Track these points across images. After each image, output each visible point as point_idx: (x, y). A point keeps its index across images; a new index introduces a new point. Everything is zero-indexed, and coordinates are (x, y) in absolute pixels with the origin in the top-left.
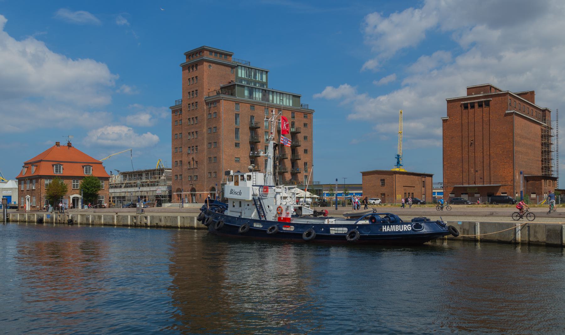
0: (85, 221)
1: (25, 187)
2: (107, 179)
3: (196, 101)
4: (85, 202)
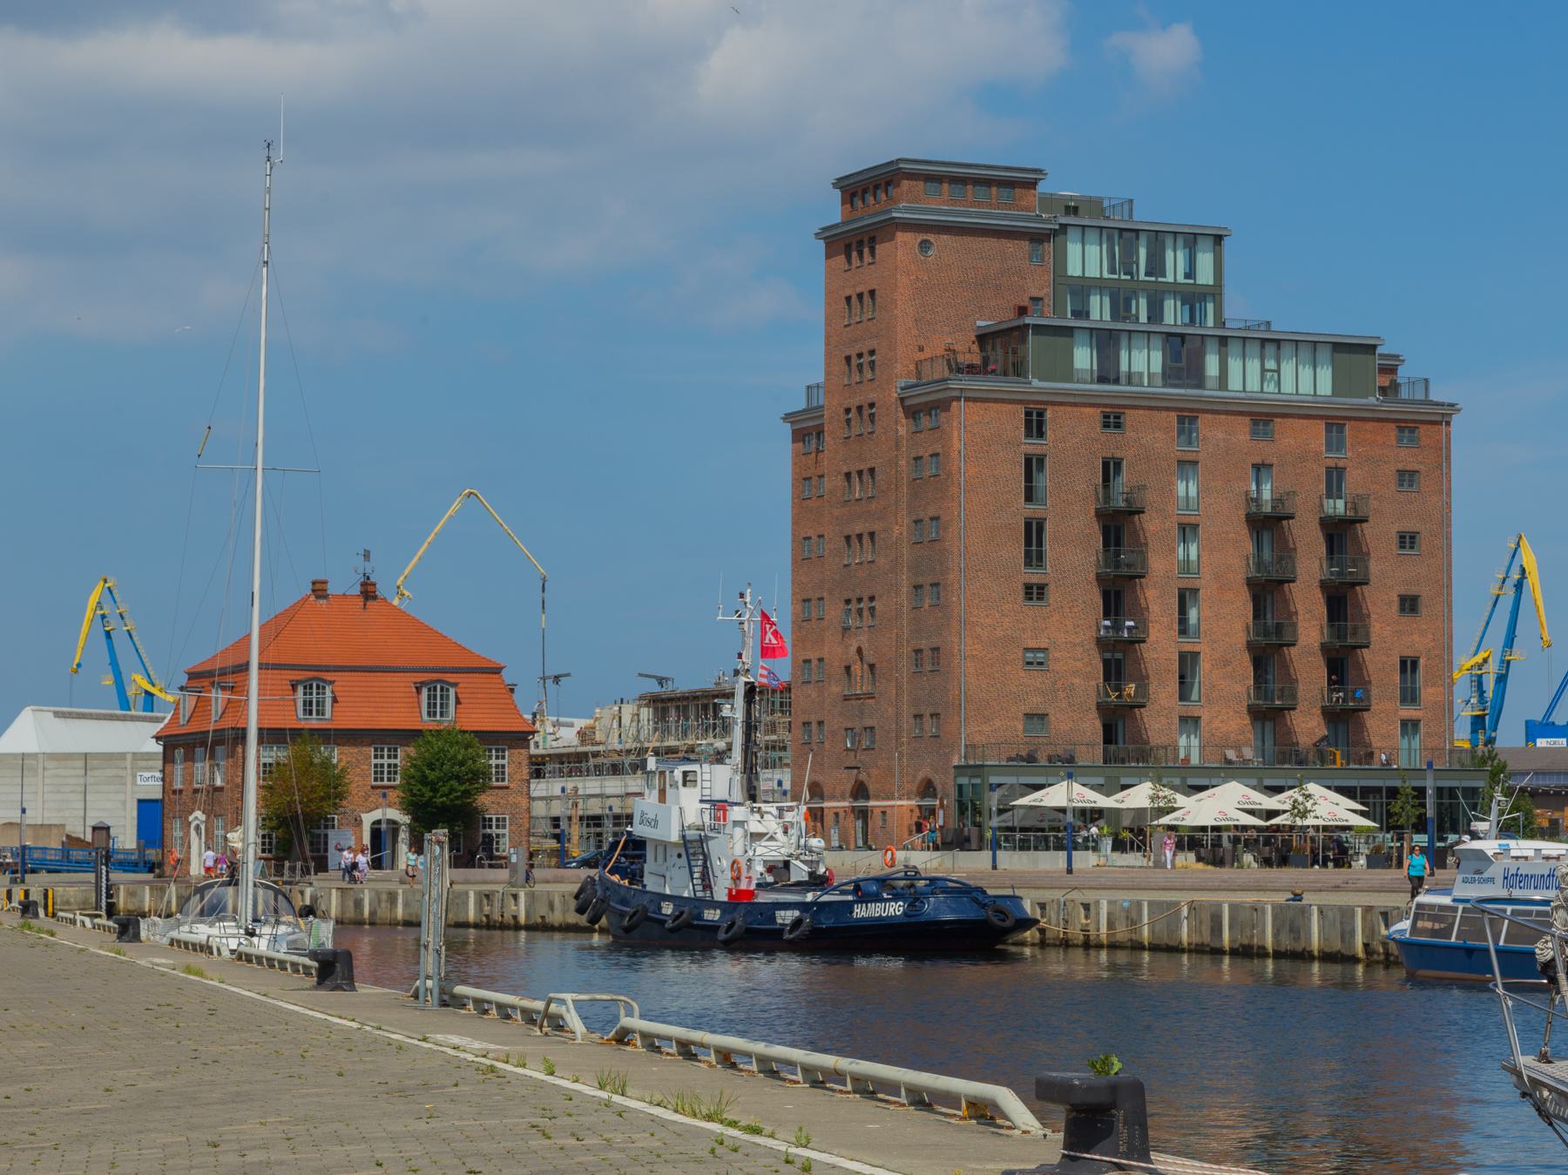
0: (350, 913)
1: (189, 777)
2: (520, 739)
3: (872, 397)
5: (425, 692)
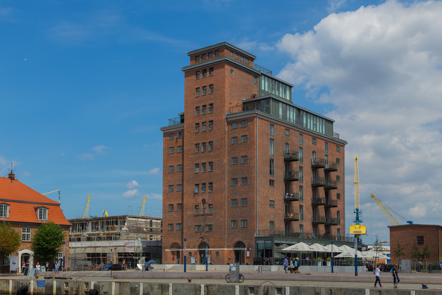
3: (211, 119)
4: (37, 260)
5: (39, 210)
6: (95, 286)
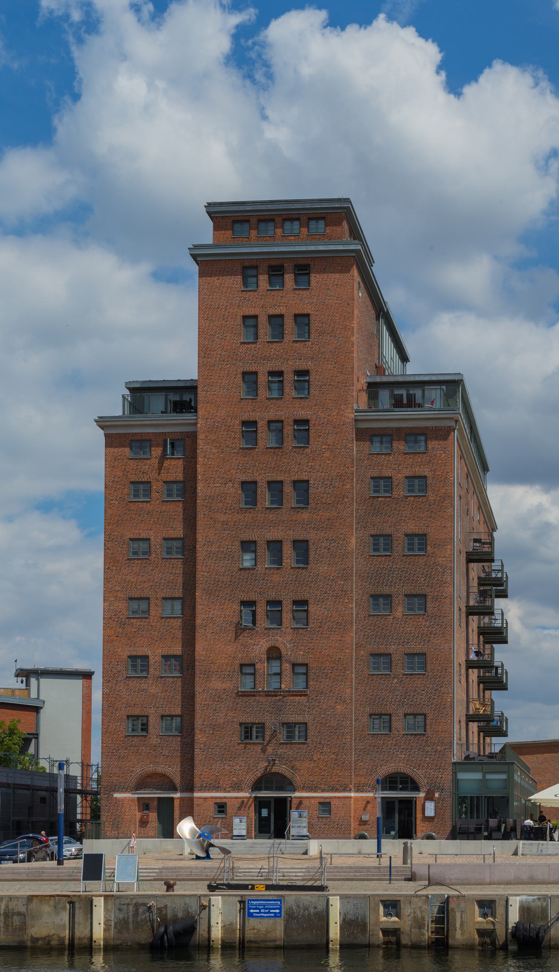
3: (302, 414)
6: (525, 910)
